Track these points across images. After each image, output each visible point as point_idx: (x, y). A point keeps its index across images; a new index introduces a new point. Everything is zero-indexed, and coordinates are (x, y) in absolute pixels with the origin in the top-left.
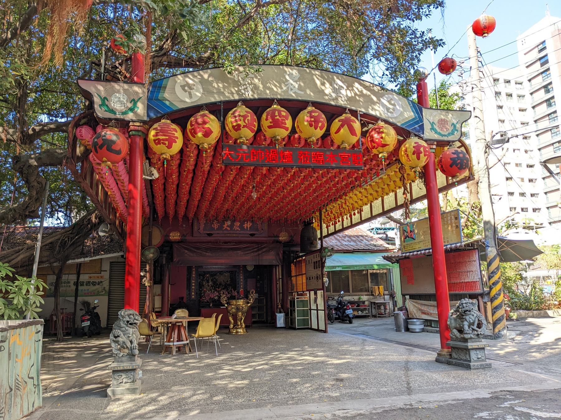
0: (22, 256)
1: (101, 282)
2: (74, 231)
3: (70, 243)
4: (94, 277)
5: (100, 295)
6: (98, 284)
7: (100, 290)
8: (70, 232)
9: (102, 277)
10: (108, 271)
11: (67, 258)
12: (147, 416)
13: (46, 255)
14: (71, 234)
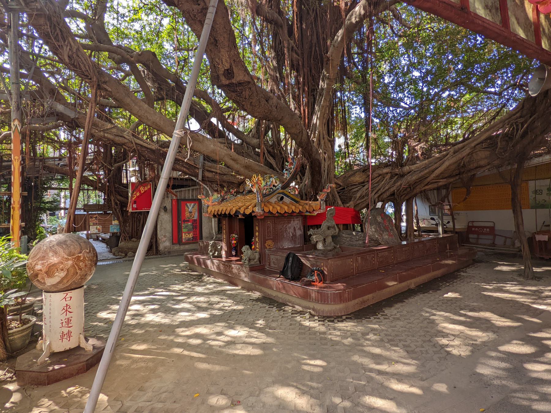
0: (447, 164)
8: (518, 115)
14: (521, 117)
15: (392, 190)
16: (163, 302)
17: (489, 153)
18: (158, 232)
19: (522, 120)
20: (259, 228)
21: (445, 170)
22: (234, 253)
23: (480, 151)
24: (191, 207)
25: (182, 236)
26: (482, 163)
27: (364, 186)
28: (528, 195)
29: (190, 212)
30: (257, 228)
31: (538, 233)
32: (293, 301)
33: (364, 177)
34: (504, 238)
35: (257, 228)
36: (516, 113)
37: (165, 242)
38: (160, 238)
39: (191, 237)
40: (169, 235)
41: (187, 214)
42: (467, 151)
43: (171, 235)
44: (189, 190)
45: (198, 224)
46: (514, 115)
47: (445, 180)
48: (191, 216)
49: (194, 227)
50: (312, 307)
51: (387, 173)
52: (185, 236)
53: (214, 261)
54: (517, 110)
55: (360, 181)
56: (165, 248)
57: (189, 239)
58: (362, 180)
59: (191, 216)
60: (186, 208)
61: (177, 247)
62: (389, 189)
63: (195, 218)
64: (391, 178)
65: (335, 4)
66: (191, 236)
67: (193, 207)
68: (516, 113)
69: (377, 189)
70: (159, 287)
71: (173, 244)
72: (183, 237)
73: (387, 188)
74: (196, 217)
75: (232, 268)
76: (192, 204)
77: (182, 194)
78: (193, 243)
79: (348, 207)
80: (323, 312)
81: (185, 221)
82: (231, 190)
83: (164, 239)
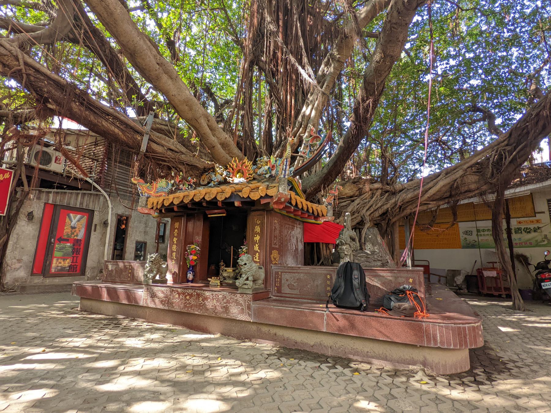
0: (441, 184)
1: (539, 228)
2: (512, 141)
3: (509, 159)
4: (526, 222)
5: (540, 246)
6: (535, 231)
7: (539, 238)
8: (506, 142)
9: (538, 221)
10: (547, 213)
11: (506, 185)
12: (14, 212)
13: (473, 180)
14: (507, 145)
15: (385, 207)
16: (63, 377)
17: (478, 177)
18: (8, 252)
19: (509, 148)
20: (262, 230)
21: (438, 191)
22: (190, 276)
23: (470, 174)
24: (75, 222)
25: (51, 264)
26: (473, 187)
27: (353, 201)
28: (459, 236)
29: (73, 228)
30: (258, 229)
31: (486, 269)
32: (366, 350)
33: (355, 189)
34: (438, 277)
35: (258, 229)
36: (504, 141)
37: (16, 269)
38: (9, 262)
39: (67, 265)
40: (27, 258)
41: (67, 230)
42: (460, 173)
43: (31, 259)
44: (78, 194)
45: (82, 246)
46: (503, 142)
47: (434, 202)
48: (73, 233)
49: (75, 251)
50: (421, 359)
51: (377, 189)
52: (56, 264)
53: (156, 289)
54: (505, 138)
55: (349, 195)
56: (16, 280)
57: (63, 269)
58: (352, 194)
59: (73, 233)
60: (67, 220)
61: (38, 280)
62: (381, 206)
63: (79, 238)
64: (382, 195)
65: (318, 10)
66: (67, 263)
67: (78, 221)
68: (504, 141)
69: (369, 205)
70: (31, 342)
71: (32, 274)
72: (54, 265)
73: (380, 205)
74: (81, 235)
75: (205, 299)
76: (79, 216)
77: (64, 199)
78: (69, 275)
79: (338, 223)
80: (444, 366)
81: (61, 240)
82: (189, 178)
83: (18, 265)
